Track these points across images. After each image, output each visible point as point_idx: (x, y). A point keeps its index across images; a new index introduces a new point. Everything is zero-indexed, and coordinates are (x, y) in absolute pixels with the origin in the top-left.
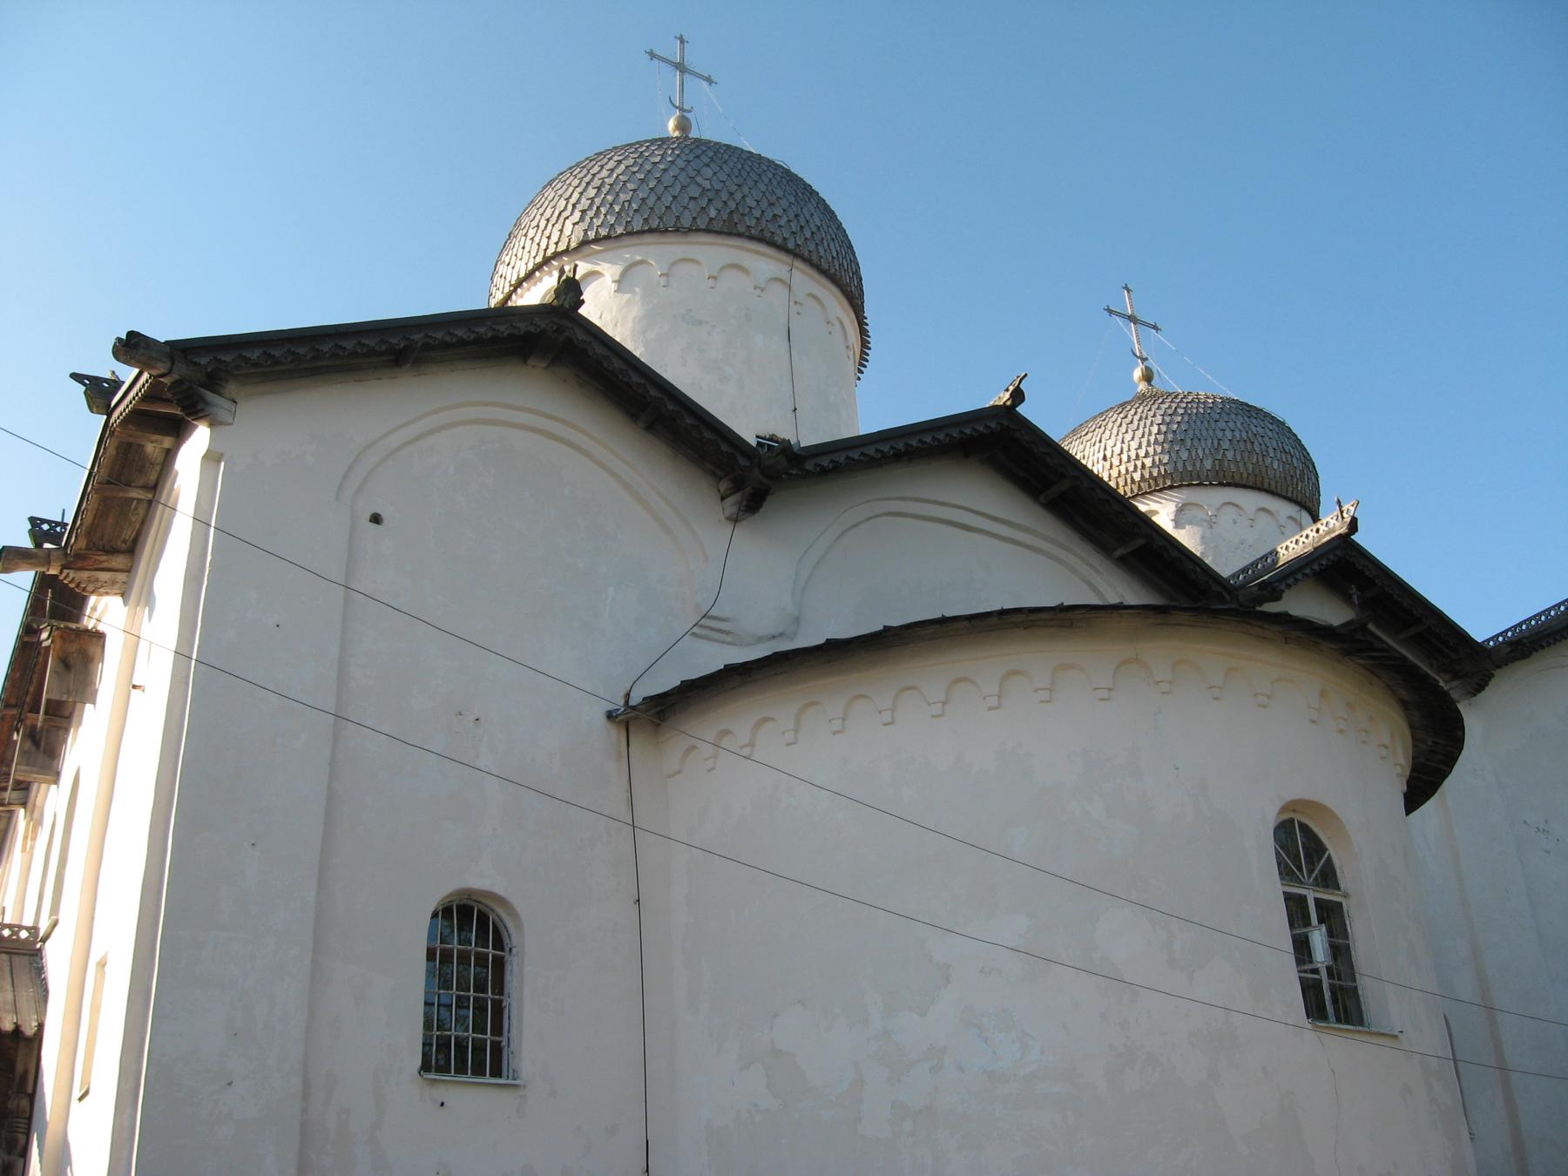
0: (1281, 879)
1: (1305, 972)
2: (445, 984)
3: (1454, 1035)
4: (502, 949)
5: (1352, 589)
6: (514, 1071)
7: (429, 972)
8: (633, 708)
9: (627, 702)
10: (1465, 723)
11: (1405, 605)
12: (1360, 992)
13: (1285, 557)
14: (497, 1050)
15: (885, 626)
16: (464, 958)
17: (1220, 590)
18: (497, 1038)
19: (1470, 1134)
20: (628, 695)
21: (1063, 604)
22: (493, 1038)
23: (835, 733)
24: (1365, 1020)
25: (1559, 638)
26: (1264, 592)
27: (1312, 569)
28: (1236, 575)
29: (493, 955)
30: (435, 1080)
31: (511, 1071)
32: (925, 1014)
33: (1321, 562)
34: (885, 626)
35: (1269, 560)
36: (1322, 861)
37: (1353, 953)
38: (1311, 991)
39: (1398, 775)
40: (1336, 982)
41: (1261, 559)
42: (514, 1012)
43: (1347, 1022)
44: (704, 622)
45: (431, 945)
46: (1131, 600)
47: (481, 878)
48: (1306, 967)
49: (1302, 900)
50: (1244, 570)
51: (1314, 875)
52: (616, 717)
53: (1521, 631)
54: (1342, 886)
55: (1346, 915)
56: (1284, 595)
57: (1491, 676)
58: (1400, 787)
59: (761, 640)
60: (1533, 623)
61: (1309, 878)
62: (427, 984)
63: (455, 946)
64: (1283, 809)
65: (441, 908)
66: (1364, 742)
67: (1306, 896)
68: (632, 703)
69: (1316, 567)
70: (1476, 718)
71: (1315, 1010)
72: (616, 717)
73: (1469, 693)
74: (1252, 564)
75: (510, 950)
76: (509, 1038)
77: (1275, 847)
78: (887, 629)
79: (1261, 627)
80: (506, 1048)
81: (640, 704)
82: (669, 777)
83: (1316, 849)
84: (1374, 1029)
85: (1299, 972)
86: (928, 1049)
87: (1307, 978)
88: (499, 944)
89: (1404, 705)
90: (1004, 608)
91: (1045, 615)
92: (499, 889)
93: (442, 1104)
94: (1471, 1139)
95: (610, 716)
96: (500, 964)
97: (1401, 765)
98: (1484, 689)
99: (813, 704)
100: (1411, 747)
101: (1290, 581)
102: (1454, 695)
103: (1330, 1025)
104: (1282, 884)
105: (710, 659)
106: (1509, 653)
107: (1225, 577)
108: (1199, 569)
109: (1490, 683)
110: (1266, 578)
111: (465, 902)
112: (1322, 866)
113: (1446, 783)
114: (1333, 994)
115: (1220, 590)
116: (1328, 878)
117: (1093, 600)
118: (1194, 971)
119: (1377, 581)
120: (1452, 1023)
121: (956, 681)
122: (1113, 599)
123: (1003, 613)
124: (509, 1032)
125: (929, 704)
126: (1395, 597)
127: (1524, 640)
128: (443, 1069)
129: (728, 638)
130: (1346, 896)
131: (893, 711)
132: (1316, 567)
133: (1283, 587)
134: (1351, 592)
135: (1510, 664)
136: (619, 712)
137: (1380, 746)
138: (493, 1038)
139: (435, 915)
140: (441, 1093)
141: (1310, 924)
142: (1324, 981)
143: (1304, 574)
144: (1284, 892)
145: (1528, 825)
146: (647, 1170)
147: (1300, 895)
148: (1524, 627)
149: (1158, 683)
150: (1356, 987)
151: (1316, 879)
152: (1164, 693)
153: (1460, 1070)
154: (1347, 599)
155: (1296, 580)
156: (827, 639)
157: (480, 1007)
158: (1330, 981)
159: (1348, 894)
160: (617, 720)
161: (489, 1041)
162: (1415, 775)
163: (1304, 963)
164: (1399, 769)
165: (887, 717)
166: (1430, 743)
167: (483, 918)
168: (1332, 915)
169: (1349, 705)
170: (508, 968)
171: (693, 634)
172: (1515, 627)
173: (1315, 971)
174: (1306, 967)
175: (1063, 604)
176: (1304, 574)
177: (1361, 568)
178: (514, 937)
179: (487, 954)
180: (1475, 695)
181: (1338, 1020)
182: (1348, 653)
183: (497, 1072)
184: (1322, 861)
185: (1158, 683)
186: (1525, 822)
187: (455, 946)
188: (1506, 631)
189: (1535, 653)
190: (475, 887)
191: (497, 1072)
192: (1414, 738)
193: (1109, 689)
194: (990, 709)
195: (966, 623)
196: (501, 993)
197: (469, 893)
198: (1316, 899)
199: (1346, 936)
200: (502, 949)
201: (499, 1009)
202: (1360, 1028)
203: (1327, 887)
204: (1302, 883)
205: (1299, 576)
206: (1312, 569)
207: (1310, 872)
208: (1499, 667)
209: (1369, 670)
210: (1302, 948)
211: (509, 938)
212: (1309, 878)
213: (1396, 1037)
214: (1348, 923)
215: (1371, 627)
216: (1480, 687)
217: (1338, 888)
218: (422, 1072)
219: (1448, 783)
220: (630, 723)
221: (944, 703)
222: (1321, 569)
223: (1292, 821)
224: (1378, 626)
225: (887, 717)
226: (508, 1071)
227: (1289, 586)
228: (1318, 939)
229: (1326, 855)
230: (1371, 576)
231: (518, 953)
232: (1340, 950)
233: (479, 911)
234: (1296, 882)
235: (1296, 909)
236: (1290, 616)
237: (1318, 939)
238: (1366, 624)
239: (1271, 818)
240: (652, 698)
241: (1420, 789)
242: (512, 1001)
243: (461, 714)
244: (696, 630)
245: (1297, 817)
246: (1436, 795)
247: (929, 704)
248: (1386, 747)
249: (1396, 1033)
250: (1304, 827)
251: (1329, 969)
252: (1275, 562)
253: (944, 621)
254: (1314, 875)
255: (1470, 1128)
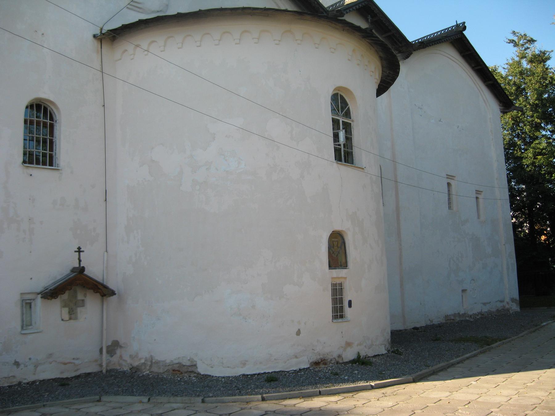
0: (333, 110)
1: (336, 145)
2: (31, 132)
3: (382, 172)
4: (53, 121)
5: (368, 16)
6: (58, 164)
7: (26, 128)
8: (104, 34)
9: (101, 32)
10: (400, 67)
11: (386, 25)
12: (353, 153)
13: (347, 2)
14: (51, 157)
15: (200, 10)
16: (38, 123)
17: (322, 11)
18: (51, 153)
19: (383, 204)
20: (101, 29)
21: (265, 7)
22: (50, 152)
23: (179, 48)
24: (354, 162)
25: (436, 43)
26: (338, 14)
27: (356, 8)
28: (329, 7)
29: (49, 123)
30: (28, 166)
31: (56, 164)
32: (205, 150)
33: (360, 5)
34: (200, 10)
35: (341, 3)
36: (346, 109)
37: (353, 140)
38: (337, 151)
39: (376, 82)
40: (346, 149)
41: (339, 2)
42: (57, 146)
43: (348, 163)
44: (131, 3)
45: (26, 118)
46: (289, 9)
47: (45, 94)
48: (337, 143)
49: (338, 121)
50: (332, 6)
51: (343, 113)
52: (97, 37)
53: (424, 40)
54: (352, 118)
55: (352, 128)
56: (345, 16)
57: (411, 53)
58: (376, 87)
59: (153, 12)
60: (429, 37)
61: (341, 114)
62: (25, 133)
63: (35, 119)
64: (335, 90)
65: (29, 105)
66: (366, 69)
67: (339, 120)
68: (104, 32)
69: (357, 7)
70: (405, 68)
71: (338, 158)
72: (97, 37)
73: (403, 58)
74: (335, 4)
75: (56, 121)
76: (56, 153)
77: (331, 103)
78: (200, 11)
79: (335, 24)
80: (55, 156)
81: (106, 32)
82: (117, 61)
83: (344, 103)
84: (356, 166)
85: (334, 145)
86: (206, 162)
87: (336, 147)
88: (52, 119)
89: (381, 58)
90: (244, 7)
91: (258, 11)
92: (51, 99)
93: (31, 175)
94: (383, 205)
95: (95, 36)
96: (52, 127)
97: (377, 79)
98: (408, 58)
99: (172, 37)
100: (381, 73)
101: (348, 11)
102: (399, 58)
103: (343, 163)
104: (332, 115)
105: (133, 17)
106: (419, 46)
107: (326, 7)
108: (316, 3)
109: (411, 56)
110: (339, 8)
111: (38, 103)
112: (346, 110)
113: (392, 87)
114: (345, 153)
115: (322, 11)
116: (348, 114)
117: (276, 8)
118: (299, 142)
119: (378, 15)
120: (383, 169)
121: (224, 33)
122: (283, 8)
123: (244, 9)
124: (56, 151)
125: (214, 40)
126: (383, 21)
127: (425, 42)
128: (31, 162)
129: (141, 11)
130: (353, 121)
131: (201, 41)
132: (357, 7)
133: (345, 12)
134: (368, 17)
135: (418, 50)
136: (98, 35)
137: (371, 71)
138: (50, 152)
139: (27, 107)
140: (30, 171)
141: (340, 129)
142: (342, 149)
143: (353, 9)
144: (332, 118)
145: (416, 106)
146: (106, 200)
147: (337, 119)
148: (425, 38)
149: (297, 40)
150: (352, 152)
151: (343, 114)
152: (298, 44)
153: (383, 181)
154: (367, 20)
155: (350, 11)
156: (178, 13)
157: (45, 141)
158: (344, 149)
159: (353, 120)
160: (97, 38)
161: (48, 154)
162: (381, 83)
163: (336, 142)
164: (376, 80)
165: (198, 44)
166: (388, 73)
167: (46, 109)
168: (348, 127)
169: (362, 55)
170: (55, 127)
171: (128, 8)
172: (422, 38)
173: (340, 145)
174: (337, 143)
175: (265, 7)
176: (353, 9)
177: (373, 9)
178: (57, 117)
179: (47, 153)
180: (405, 59)
181: (345, 162)
182: (364, 37)
183: (51, 164)
184: (346, 109)
185: (297, 40)
186: (415, 105)
187: (35, 119)
188: (419, 39)
189: (427, 47)
190: (42, 97)
191: (51, 164)
192: (383, 71)
193: (279, 41)
194: (236, 44)
195: (229, 11)
196: (53, 136)
197: (40, 99)
198: (342, 121)
199: (351, 135)
200: (53, 121)
201: (52, 142)
202: (352, 165)
203: (347, 117)
204: (339, 115)
205: (351, 10)
206: (356, 8)
207: (342, 112)
208: (415, 51)
209: (370, 44)
210: (336, 137)
211: (56, 117)
212: (341, 114)
213: (363, 169)
214: (352, 131)
215: (373, 31)
216: (407, 57)
217: (350, 118)
218: (23, 163)
219: (392, 88)
220: (102, 40)
221: (219, 40)
222: (359, 8)
223: (338, 94)
224: (376, 31)
225: (198, 44)
226: (55, 164)
227: (347, 13)
228: (342, 135)
229: (348, 107)
230: (376, 13)
231: (59, 122)
232: (349, 139)
233: (44, 106)
234: (337, 115)
235: (335, 123)
236: (346, 21)
237: (342, 135)
238: (372, 30)
239: (331, 92)
240: (111, 31)
241: (382, 89)
242: (56, 140)
243: (36, 32)
244: (128, 6)
245: (340, 93)
246: (387, 91)
247: (214, 40)
248: (373, 72)
249: (363, 168)
250: (342, 97)
251: (344, 145)
252: (343, 4)
253: (221, 10)
254: (343, 113)
255: (383, 202)
